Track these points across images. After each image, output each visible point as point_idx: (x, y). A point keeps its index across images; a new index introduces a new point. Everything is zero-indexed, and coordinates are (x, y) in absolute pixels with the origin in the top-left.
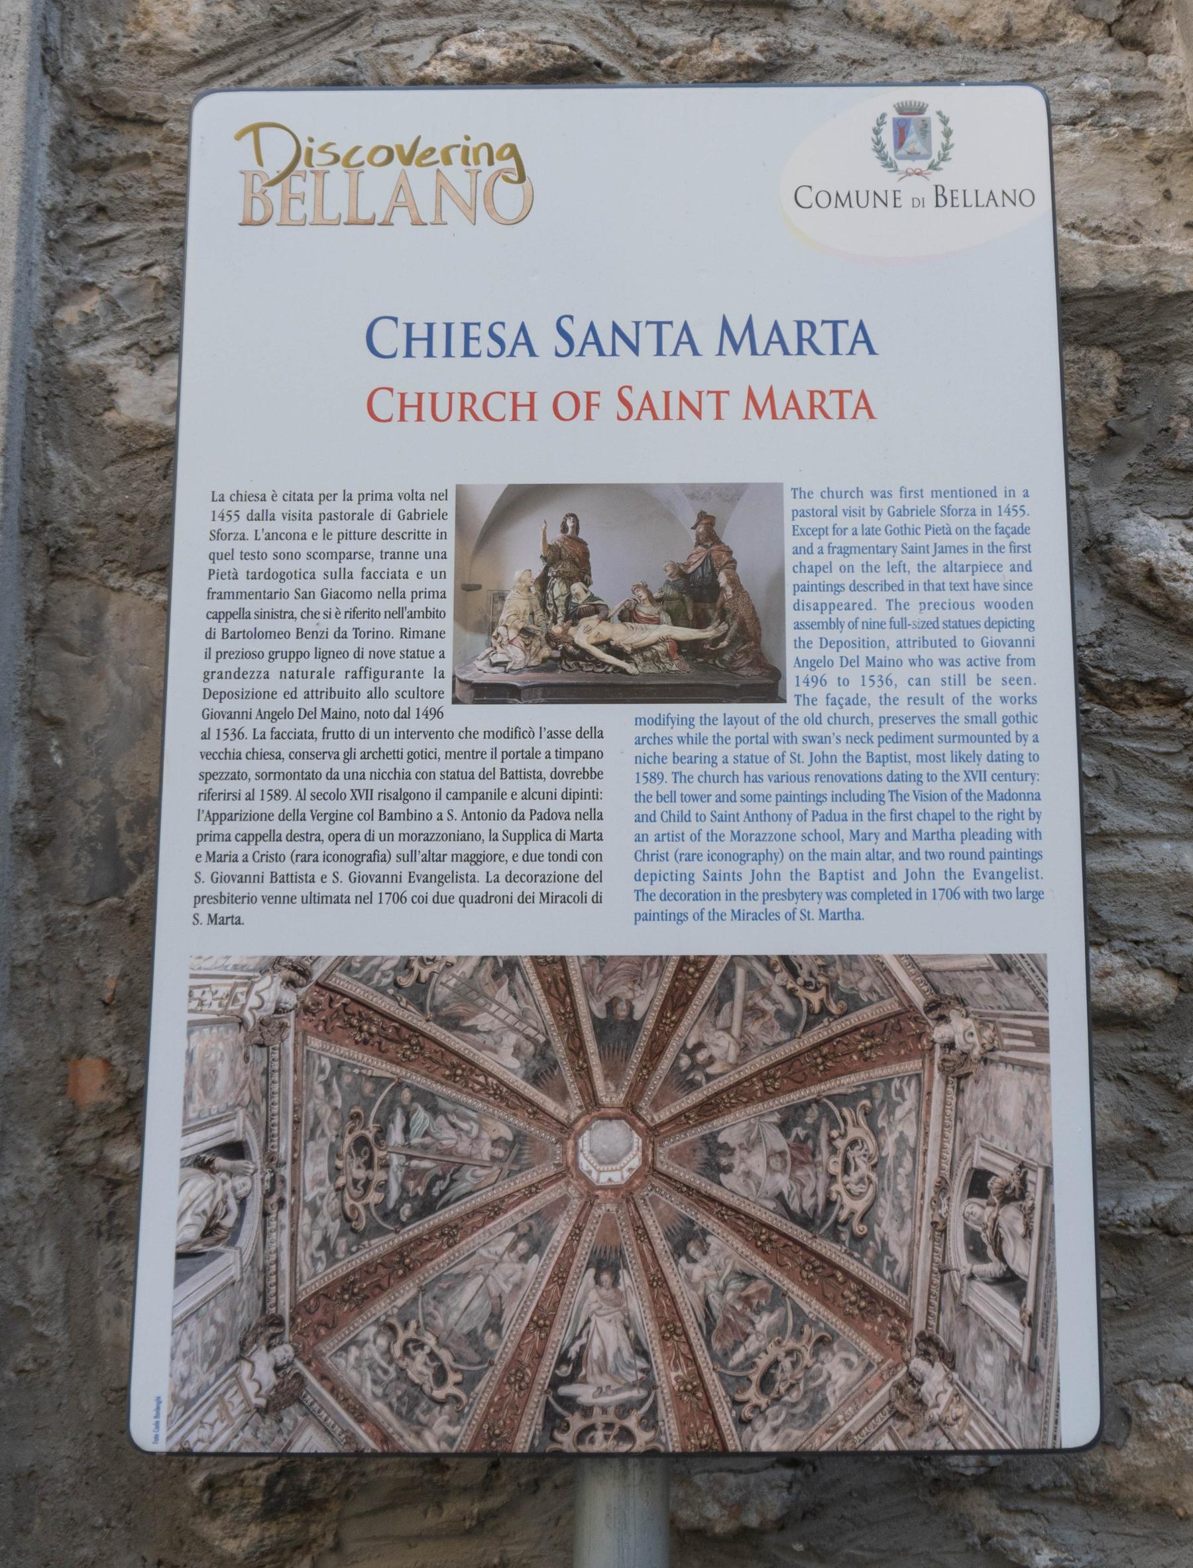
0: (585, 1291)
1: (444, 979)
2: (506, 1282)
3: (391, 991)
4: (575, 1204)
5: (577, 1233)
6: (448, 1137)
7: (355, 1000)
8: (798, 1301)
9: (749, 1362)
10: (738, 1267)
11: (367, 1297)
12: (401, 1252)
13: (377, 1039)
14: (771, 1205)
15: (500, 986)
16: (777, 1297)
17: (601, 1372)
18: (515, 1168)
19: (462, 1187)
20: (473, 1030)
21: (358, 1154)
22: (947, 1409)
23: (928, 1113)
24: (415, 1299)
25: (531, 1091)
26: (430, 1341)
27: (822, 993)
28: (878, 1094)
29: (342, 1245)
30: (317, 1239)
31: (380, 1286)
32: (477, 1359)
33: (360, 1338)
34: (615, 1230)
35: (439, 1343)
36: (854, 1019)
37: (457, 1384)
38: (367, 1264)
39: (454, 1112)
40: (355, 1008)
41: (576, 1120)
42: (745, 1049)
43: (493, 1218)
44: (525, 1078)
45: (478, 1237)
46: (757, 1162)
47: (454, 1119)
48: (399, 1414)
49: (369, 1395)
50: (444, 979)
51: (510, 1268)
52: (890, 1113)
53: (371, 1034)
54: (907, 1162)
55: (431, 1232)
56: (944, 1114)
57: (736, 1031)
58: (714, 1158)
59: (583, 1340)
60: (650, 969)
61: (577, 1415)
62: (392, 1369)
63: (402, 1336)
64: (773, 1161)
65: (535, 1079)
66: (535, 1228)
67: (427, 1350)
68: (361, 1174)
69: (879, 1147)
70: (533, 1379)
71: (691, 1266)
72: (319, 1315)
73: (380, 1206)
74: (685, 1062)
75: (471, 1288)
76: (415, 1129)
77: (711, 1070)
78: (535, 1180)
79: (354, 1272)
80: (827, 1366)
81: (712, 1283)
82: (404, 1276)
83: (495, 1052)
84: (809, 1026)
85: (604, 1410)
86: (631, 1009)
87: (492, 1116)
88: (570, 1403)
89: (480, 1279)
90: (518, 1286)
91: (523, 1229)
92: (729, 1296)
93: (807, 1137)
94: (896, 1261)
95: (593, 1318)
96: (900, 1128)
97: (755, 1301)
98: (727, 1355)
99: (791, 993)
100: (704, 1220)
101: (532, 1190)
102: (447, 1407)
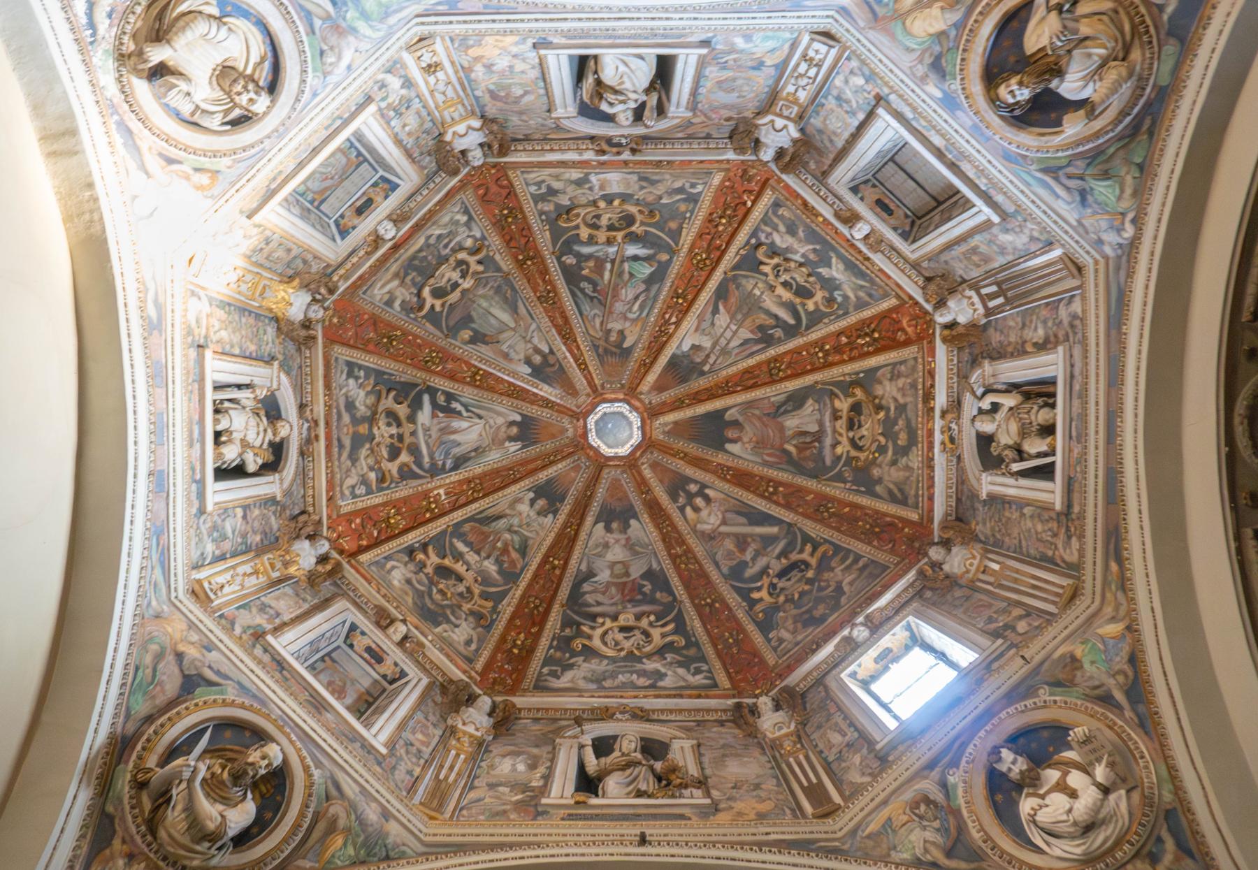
0: (505, 413)
1: (760, 285)
2: (510, 346)
3: (753, 241)
4: (570, 403)
5: (547, 404)
6: (628, 293)
7: (749, 211)
8: (510, 594)
9: (458, 557)
10: (530, 542)
11: (503, 229)
12: (537, 256)
13: (713, 231)
14: (584, 567)
15: (752, 332)
16: (511, 577)
17: (441, 430)
18: (600, 350)
19: (586, 307)
20: (716, 311)
21: (620, 219)
22: (465, 733)
23: (690, 697)
24: (499, 269)
25: (663, 360)
26: (467, 284)
28: (692, 652)
29: (549, 207)
30: (557, 185)
31: (511, 239)
32: (451, 323)
33: (473, 224)
34: (553, 436)
35: (464, 292)
36: (751, 628)
37: (433, 307)
38: (529, 229)
39: (647, 297)
40: (741, 212)
41: (640, 400)
42: (710, 537)
43: (560, 334)
44: (674, 356)
45: (545, 322)
46: (617, 553)
47: (641, 299)
48: (413, 257)
49: (429, 232)
50: (760, 285)
51: (520, 350)
52: (680, 664)
53: (717, 226)
54: (642, 681)
55: (550, 282)
56: (698, 710)
57: (723, 529)
58: (617, 516)
59: (465, 414)
60: (768, 455)
61: (408, 411)
62: (448, 251)
63: (472, 260)
64: (619, 566)
65: (674, 363)
66: (552, 369)
67: (460, 281)
68: (604, 221)
69: (649, 656)
70: (433, 372)
71: (527, 502)
72: (494, 189)
73: (576, 239)
74: (693, 488)
75: (505, 317)
76: (637, 266)
77: (688, 510)
78: (591, 368)
79: (525, 217)
80: (464, 624)
81: (516, 521)
82: (517, 261)
83: (696, 330)
84: (738, 590)
85: (413, 433)
86: (734, 441)
87: (643, 329)
88: (416, 405)
89: (512, 325)
90: (506, 356)
91: (551, 360)
92: (507, 536)
93: (644, 594)
94: (558, 678)
95: (483, 421)
96: (669, 673)
97: (505, 558)
98: (462, 537)
99: (764, 571)
100: (565, 509)
101: (583, 366)
102: (415, 299)
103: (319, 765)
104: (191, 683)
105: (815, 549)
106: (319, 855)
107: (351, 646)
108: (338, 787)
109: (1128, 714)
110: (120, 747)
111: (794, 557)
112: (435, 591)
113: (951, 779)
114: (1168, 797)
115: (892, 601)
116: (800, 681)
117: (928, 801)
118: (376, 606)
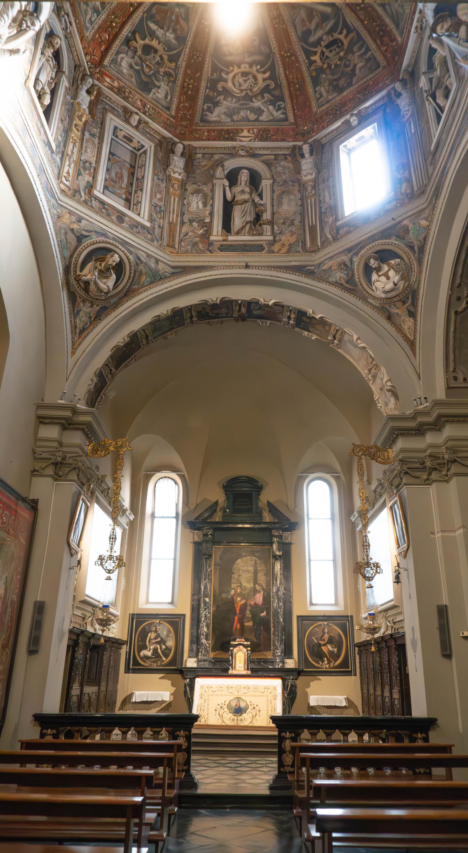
8: (184, 51)
27: (319, 63)
103: (131, 253)
104: (80, 239)
105: (349, 32)
106: (139, 283)
107: (117, 136)
108: (139, 259)
109: (416, 255)
110: (67, 270)
111: (336, 36)
112: (144, 66)
113: (354, 259)
114: (416, 287)
115: (372, 105)
116: (324, 137)
117: (345, 265)
118: (122, 106)
